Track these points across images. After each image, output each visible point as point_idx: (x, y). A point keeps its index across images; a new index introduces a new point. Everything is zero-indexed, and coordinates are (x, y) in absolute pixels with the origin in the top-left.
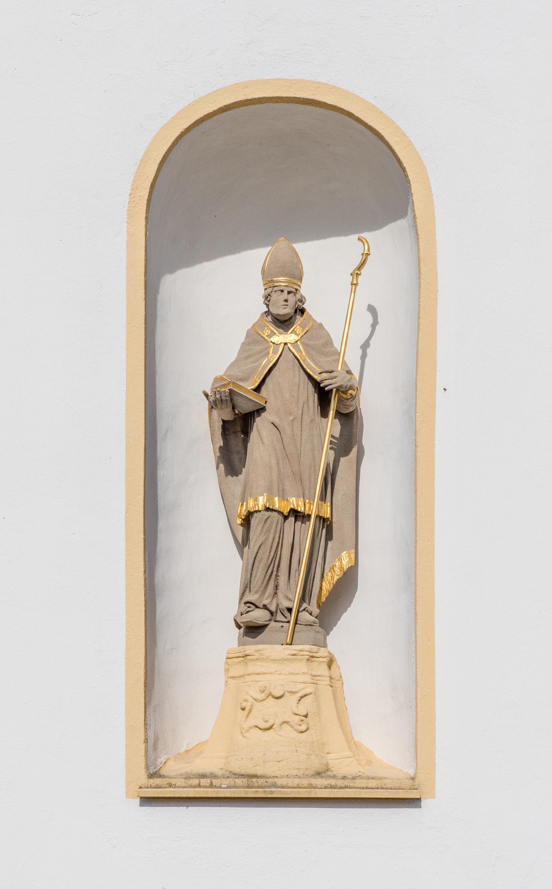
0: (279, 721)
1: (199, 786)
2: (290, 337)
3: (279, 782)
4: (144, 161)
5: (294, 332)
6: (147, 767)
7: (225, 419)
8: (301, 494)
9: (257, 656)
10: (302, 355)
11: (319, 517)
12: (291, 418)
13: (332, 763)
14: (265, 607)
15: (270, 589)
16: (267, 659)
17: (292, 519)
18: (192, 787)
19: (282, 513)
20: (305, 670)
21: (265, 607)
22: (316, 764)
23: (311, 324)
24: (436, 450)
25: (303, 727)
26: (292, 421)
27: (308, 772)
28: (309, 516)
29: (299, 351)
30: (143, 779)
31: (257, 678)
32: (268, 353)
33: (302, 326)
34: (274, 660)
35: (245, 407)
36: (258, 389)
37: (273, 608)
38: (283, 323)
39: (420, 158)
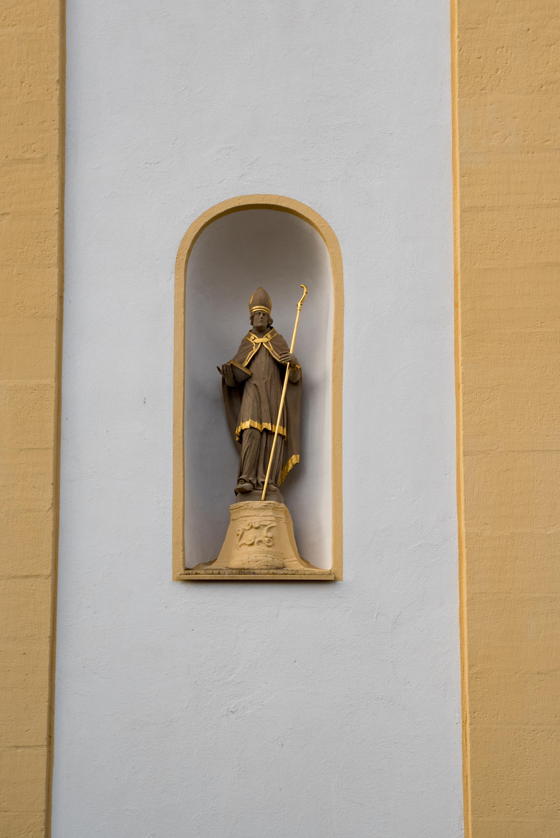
0: (257, 540)
1: (212, 574)
2: (264, 340)
3: (257, 572)
4: (184, 240)
5: (267, 337)
6: (184, 564)
7: (230, 386)
8: (270, 420)
9: (246, 507)
10: (271, 349)
11: (278, 434)
12: (265, 381)
13: (286, 564)
14: (250, 482)
15: (253, 473)
16: (251, 508)
17: (265, 435)
18: (208, 574)
19: (259, 431)
20: (271, 514)
21: (250, 482)
22: (277, 563)
23: (276, 335)
24: (343, 392)
25: (270, 544)
26: (266, 383)
27: (272, 567)
28: (274, 433)
29: (269, 346)
30: (182, 571)
31: (245, 519)
32: (252, 349)
33: (272, 334)
34: (255, 509)
35: (241, 377)
36: (248, 367)
37: (255, 482)
38: (260, 331)
39: (334, 234)
